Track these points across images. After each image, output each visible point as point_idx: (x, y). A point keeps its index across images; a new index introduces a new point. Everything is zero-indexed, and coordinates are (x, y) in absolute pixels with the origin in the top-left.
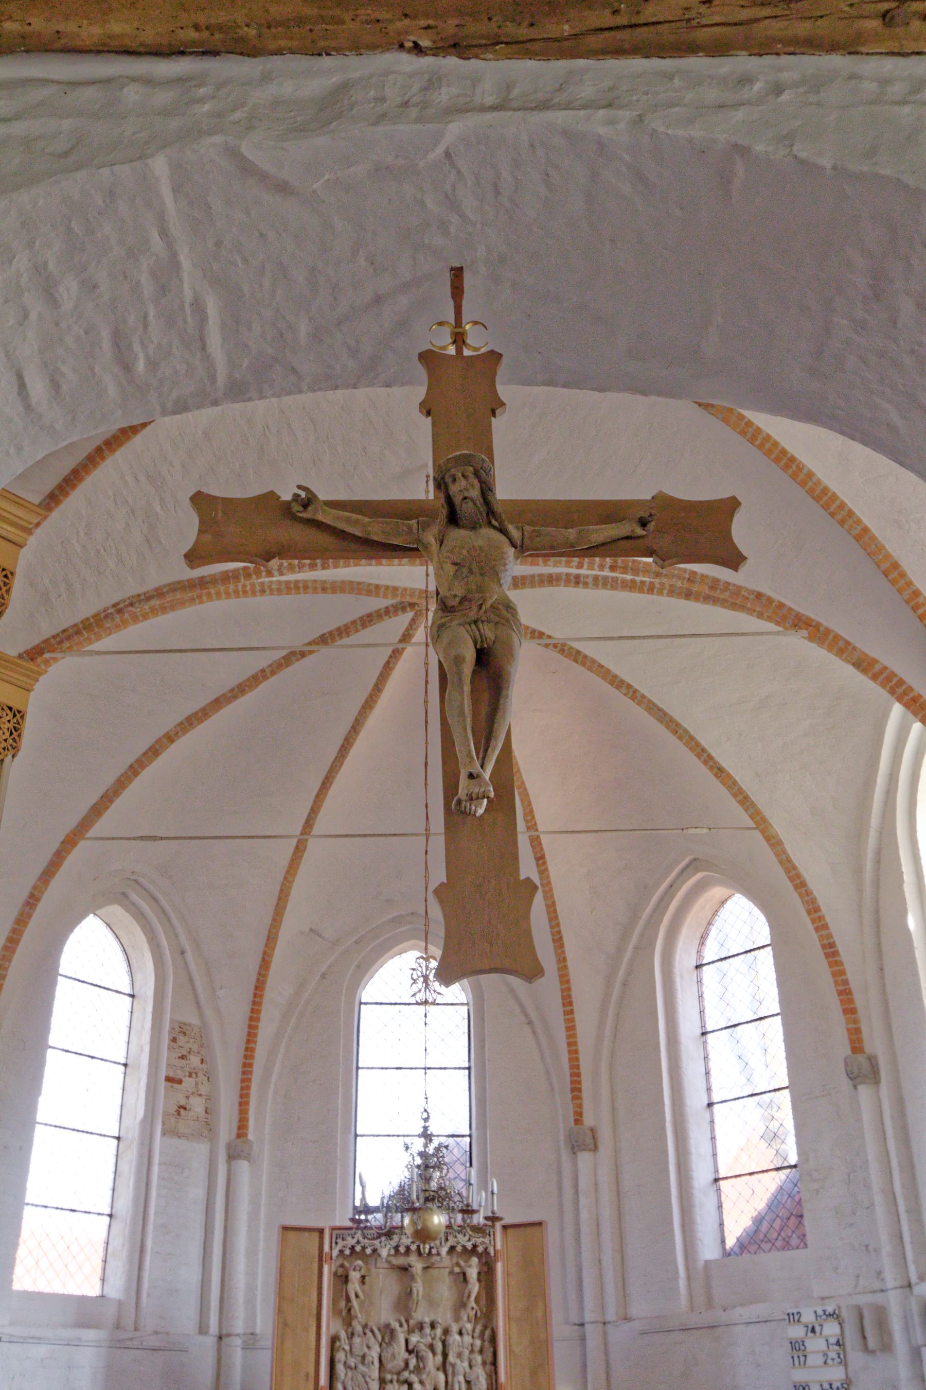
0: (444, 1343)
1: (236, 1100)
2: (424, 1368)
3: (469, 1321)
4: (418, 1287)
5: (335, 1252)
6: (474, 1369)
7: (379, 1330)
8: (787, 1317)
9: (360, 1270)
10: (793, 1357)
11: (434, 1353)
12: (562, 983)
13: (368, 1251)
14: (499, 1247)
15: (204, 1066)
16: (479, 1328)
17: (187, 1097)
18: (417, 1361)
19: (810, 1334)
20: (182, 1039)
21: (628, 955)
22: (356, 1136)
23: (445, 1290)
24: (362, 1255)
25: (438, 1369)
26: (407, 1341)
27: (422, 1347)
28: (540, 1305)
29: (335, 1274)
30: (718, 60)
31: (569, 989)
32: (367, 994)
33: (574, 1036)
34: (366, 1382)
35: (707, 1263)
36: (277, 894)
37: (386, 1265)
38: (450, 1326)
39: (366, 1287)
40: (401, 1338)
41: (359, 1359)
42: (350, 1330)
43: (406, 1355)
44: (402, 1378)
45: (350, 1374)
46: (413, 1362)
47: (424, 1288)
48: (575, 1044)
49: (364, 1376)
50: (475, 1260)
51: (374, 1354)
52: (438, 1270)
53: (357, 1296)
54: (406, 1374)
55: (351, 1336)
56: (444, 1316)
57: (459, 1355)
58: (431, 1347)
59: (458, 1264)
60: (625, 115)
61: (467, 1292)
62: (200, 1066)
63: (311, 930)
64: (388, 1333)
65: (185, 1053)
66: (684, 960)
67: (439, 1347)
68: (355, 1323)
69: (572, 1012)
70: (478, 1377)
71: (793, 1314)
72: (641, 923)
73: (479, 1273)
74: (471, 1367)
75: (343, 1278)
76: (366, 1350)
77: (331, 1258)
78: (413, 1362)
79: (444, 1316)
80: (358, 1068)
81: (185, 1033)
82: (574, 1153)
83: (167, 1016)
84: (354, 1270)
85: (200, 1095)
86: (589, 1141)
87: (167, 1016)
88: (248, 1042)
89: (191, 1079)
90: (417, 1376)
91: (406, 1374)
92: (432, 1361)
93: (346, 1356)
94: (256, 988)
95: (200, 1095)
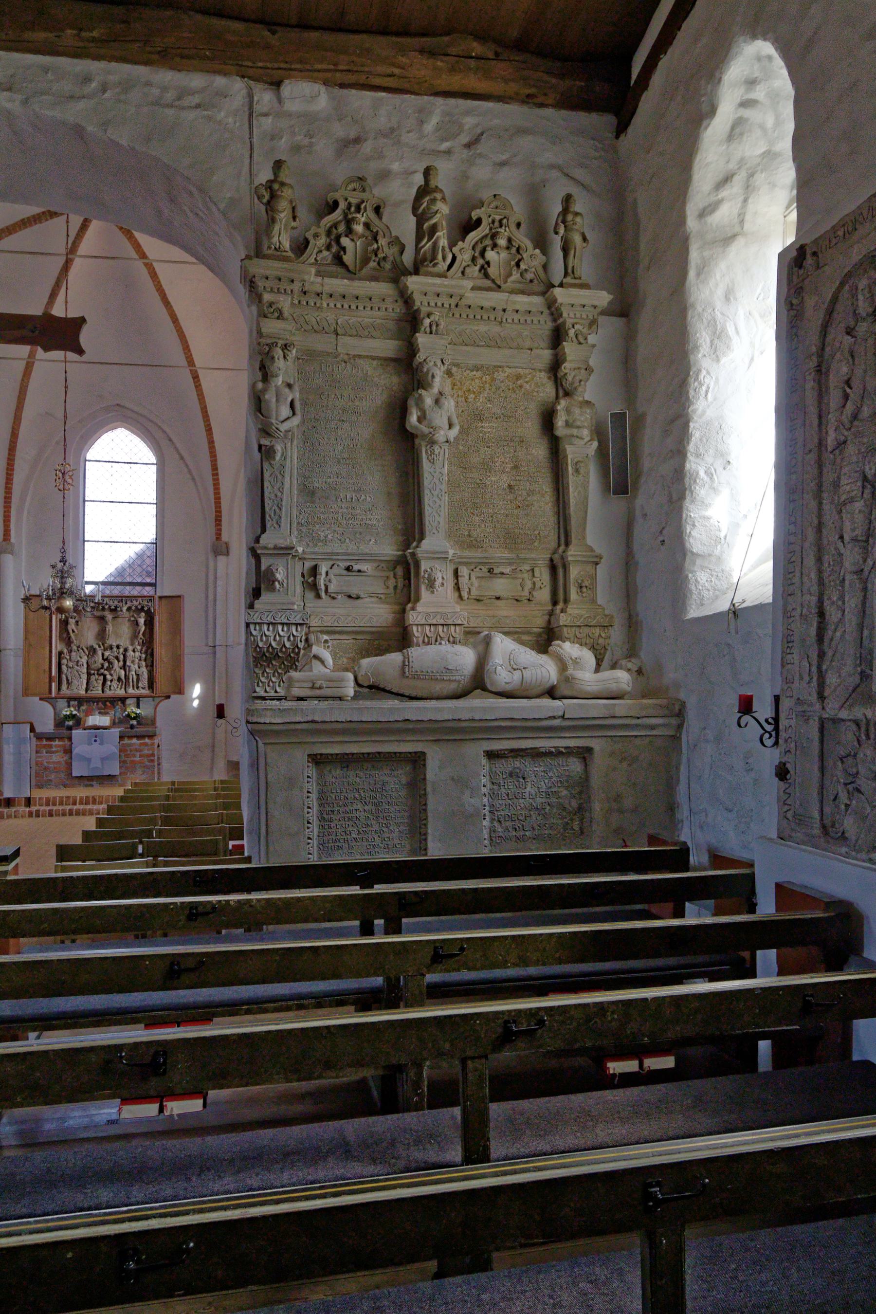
0: (124, 656)
3: (139, 644)
4: (110, 628)
11: (119, 661)
12: (211, 457)
23: (125, 629)
26: (103, 655)
27: (111, 657)
30: (75, 61)
31: (216, 460)
32: (92, 454)
39: (79, 627)
40: (100, 653)
46: (106, 665)
48: (219, 493)
50: (143, 614)
51: (84, 660)
54: (102, 671)
55: (70, 652)
56: (125, 642)
57: (133, 662)
58: (117, 658)
59: (133, 616)
60: (19, 97)
63: (46, 413)
64: (92, 651)
67: (121, 657)
68: (72, 645)
73: (145, 621)
78: (106, 665)
79: (125, 642)
86: (224, 550)
88: (7, 483)
91: (102, 671)
94: (10, 450)
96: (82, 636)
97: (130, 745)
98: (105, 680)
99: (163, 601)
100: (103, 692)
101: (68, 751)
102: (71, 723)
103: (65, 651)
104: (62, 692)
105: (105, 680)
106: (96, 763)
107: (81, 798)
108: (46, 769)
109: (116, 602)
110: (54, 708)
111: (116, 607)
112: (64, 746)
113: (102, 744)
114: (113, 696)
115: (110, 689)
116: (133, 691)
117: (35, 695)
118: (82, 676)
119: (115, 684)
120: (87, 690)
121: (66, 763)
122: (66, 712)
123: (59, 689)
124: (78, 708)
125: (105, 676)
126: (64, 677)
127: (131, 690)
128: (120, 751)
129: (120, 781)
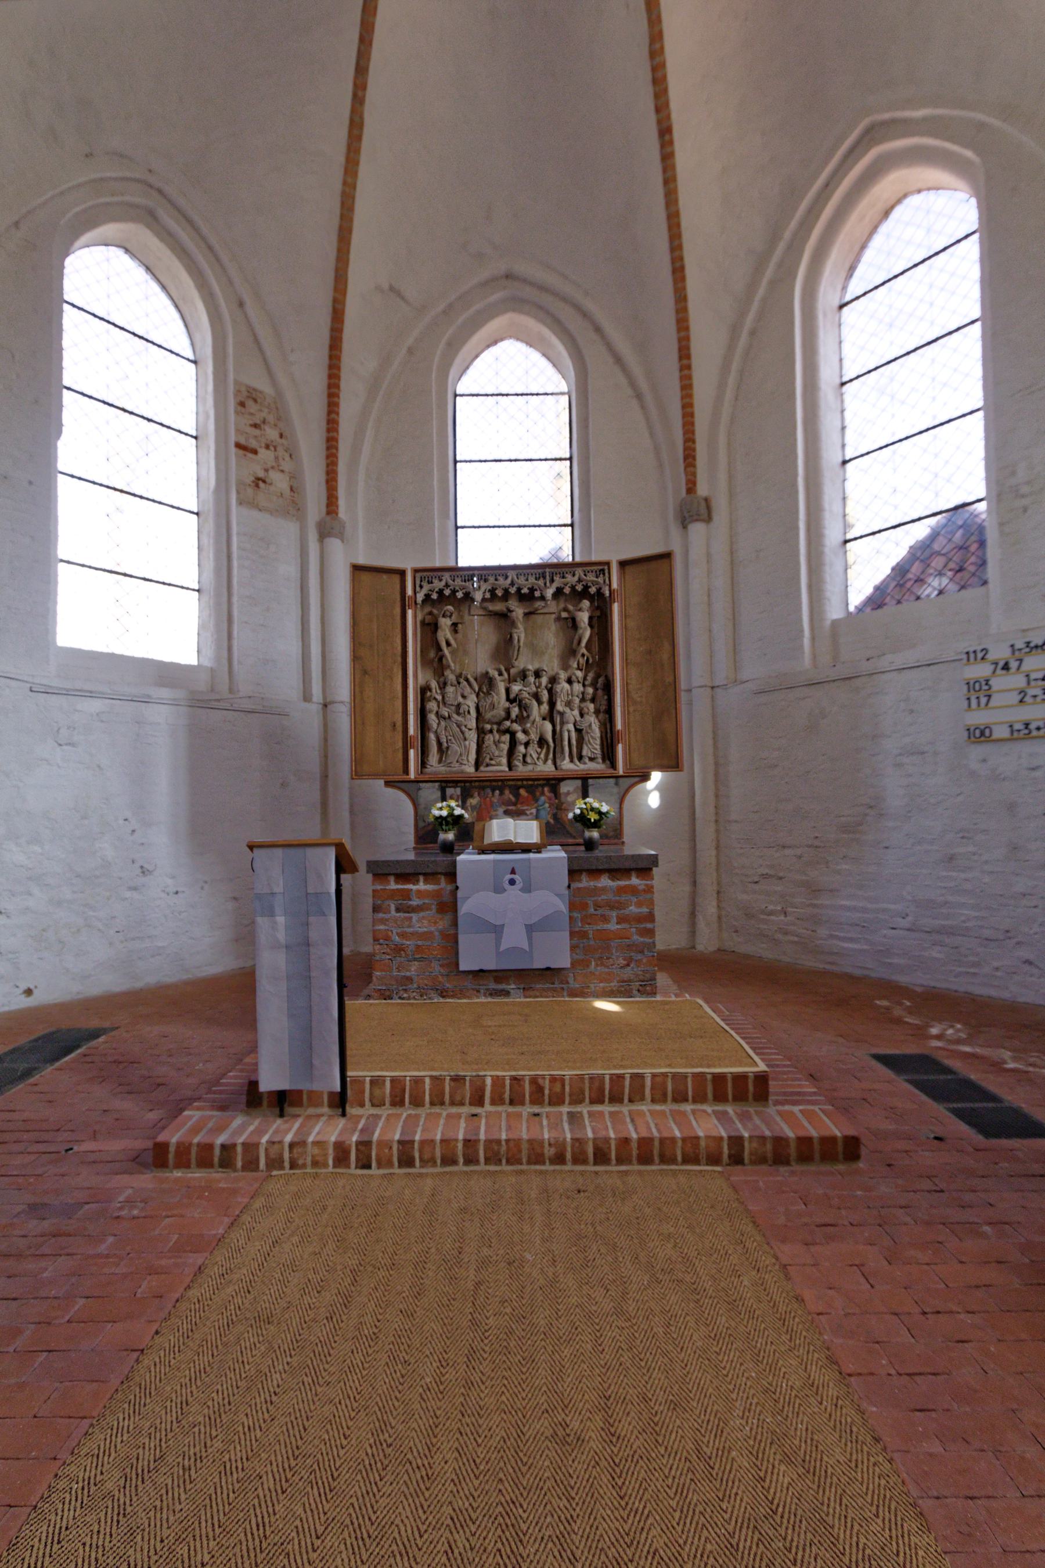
0: (550, 691)
1: (323, 478)
2: (528, 716)
4: (520, 633)
5: (420, 597)
6: (586, 717)
7: (476, 679)
8: (965, 657)
9: (450, 617)
10: (968, 699)
11: (540, 703)
13: (460, 595)
14: (615, 585)
15: (283, 441)
16: (590, 677)
17: (266, 470)
18: (520, 709)
19: (999, 672)
20: (251, 405)
21: (761, 292)
22: (457, 528)
23: (551, 637)
24: (452, 599)
25: (544, 719)
26: (508, 691)
27: (525, 695)
28: (667, 646)
29: (423, 623)
33: (690, 396)
34: (463, 733)
35: (835, 623)
36: (338, 212)
37: (481, 612)
38: (557, 674)
39: (460, 636)
40: (501, 687)
41: (453, 708)
42: (442, 679)
43: (507, 704)
44: (502, 728)
45: (443, 723)
46: (515, 711)
47: (526, 636)
48: (691, 405)
49: (459, 726)
50: (586, 604)
51: (471, 702)
52: (542, 616)
53: (448, 644)
54: (508, 723)
55: (443, 686)
56: (551, 664)
57: (569, 704)
58: (536, 697)
59: (565, 610)
61: (577, 637)
62: (279, 440)
63: (392, 288)
64: (487, 683)
65: (258, 422)
66: (827, 296)
67: (545, 696)
68: (447, 673)
69: (689, 367)
70: (590, 725)
71: (975, 652)
72: (781, 247)
73: (591, 618)
74: (582, 715)
75: (430, 627)
76: (460, 699)
77: (416, 603)
78: (515, 711)
79: (551, 664)
80: (456, 462)
81: (255, 401)
82: (685, 527)
83: (231, 377)
84: (444, 616)
85: (282, 471)
86: (703, 510)
87: (231, 377)
88: (329, 413)
89: (268, 452)
90: (520, 725)
92: (537, 711)
93: (439, 706)
95: (282, 471)
96: (466, 652)
97: (595, 891)
98: (513, 743)
99: (629, 569)
100: (510, 767)
101: (449, 906)
102: (450, 836)
103: (434, 684)
104: (429, 770)
105: (513, 743)
106: (515, 937)
107: (498, 1081)
108: (399, 949)
109: (532, 580)
110: (416, 806)
111: (532, 590)
112: (437, 894)
113: (527, 889)
114: (533, 775)
115: (525, 762)
116: (571, 766)
117: (375, 776)
118: (467, 734)
119: (533, 750)
120: (477, 765)
121: (444, 935)
122: (440, 810)
123: (423, 763)
124: (464, 800)
125: (513, 735)
126: (432, 737)
127: (566, 765)
128: (572, 907)
129: (574, 984)
